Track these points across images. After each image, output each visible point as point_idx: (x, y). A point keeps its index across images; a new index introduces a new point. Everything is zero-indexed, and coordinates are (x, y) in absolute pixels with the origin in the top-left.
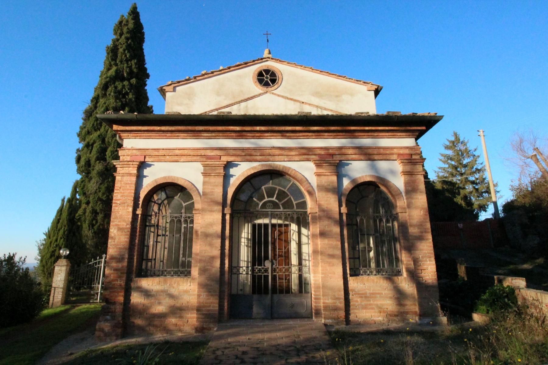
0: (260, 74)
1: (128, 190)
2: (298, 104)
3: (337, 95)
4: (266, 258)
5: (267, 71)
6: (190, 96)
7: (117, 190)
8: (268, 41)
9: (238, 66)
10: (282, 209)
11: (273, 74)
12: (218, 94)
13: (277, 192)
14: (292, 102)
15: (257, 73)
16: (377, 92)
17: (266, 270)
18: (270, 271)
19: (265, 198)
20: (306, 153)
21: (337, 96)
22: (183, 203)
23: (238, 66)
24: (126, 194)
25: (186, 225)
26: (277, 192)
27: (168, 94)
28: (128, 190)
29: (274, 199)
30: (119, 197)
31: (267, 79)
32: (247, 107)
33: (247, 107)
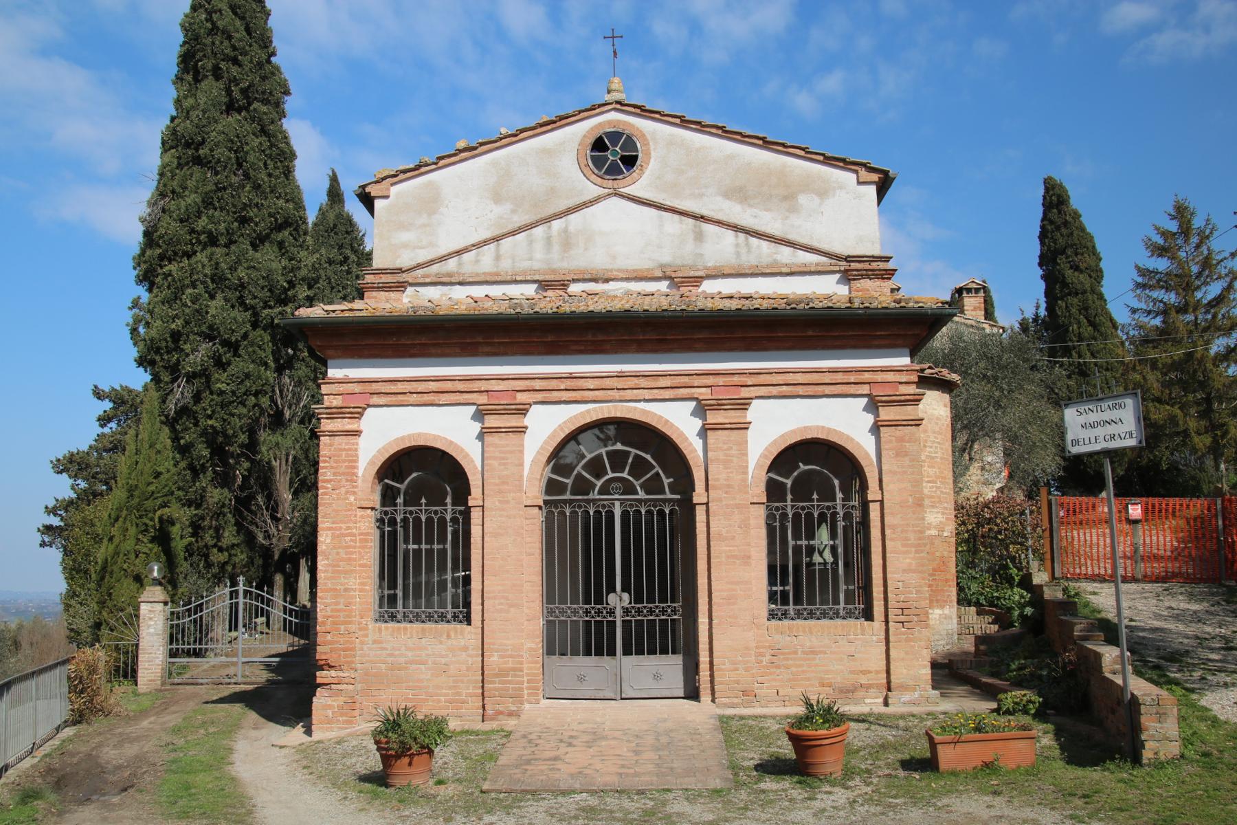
0: (599, 145)
1: (344, 461)
2: (690, 221)
3: (788, 197)
4: (612, 589)
5: (615, 136)
6: (431, 203)
7: (325, 462)
8: (615, 53)
9: (542, 125)
10: (641, 495)
11: (630, 143)
12: (497, 198)
13: (630, 460)
14: (676, 217)
15: (591, 140)
16: (884, 185)
17: (611, 612)
18: (619, 612)
19: (607, 473)
20: (675, 390)
21: (785, 198)
22: (789, 486)
23: (542, 125)
24: (342, 470)
25: (416, 547)
26: (630, 460)
27: (378, 204)
28: (344, 461)
29: (625, 475)
30: (329, 476)
31: (613, 157)
32: (566, 231)
33: (566, 231)
